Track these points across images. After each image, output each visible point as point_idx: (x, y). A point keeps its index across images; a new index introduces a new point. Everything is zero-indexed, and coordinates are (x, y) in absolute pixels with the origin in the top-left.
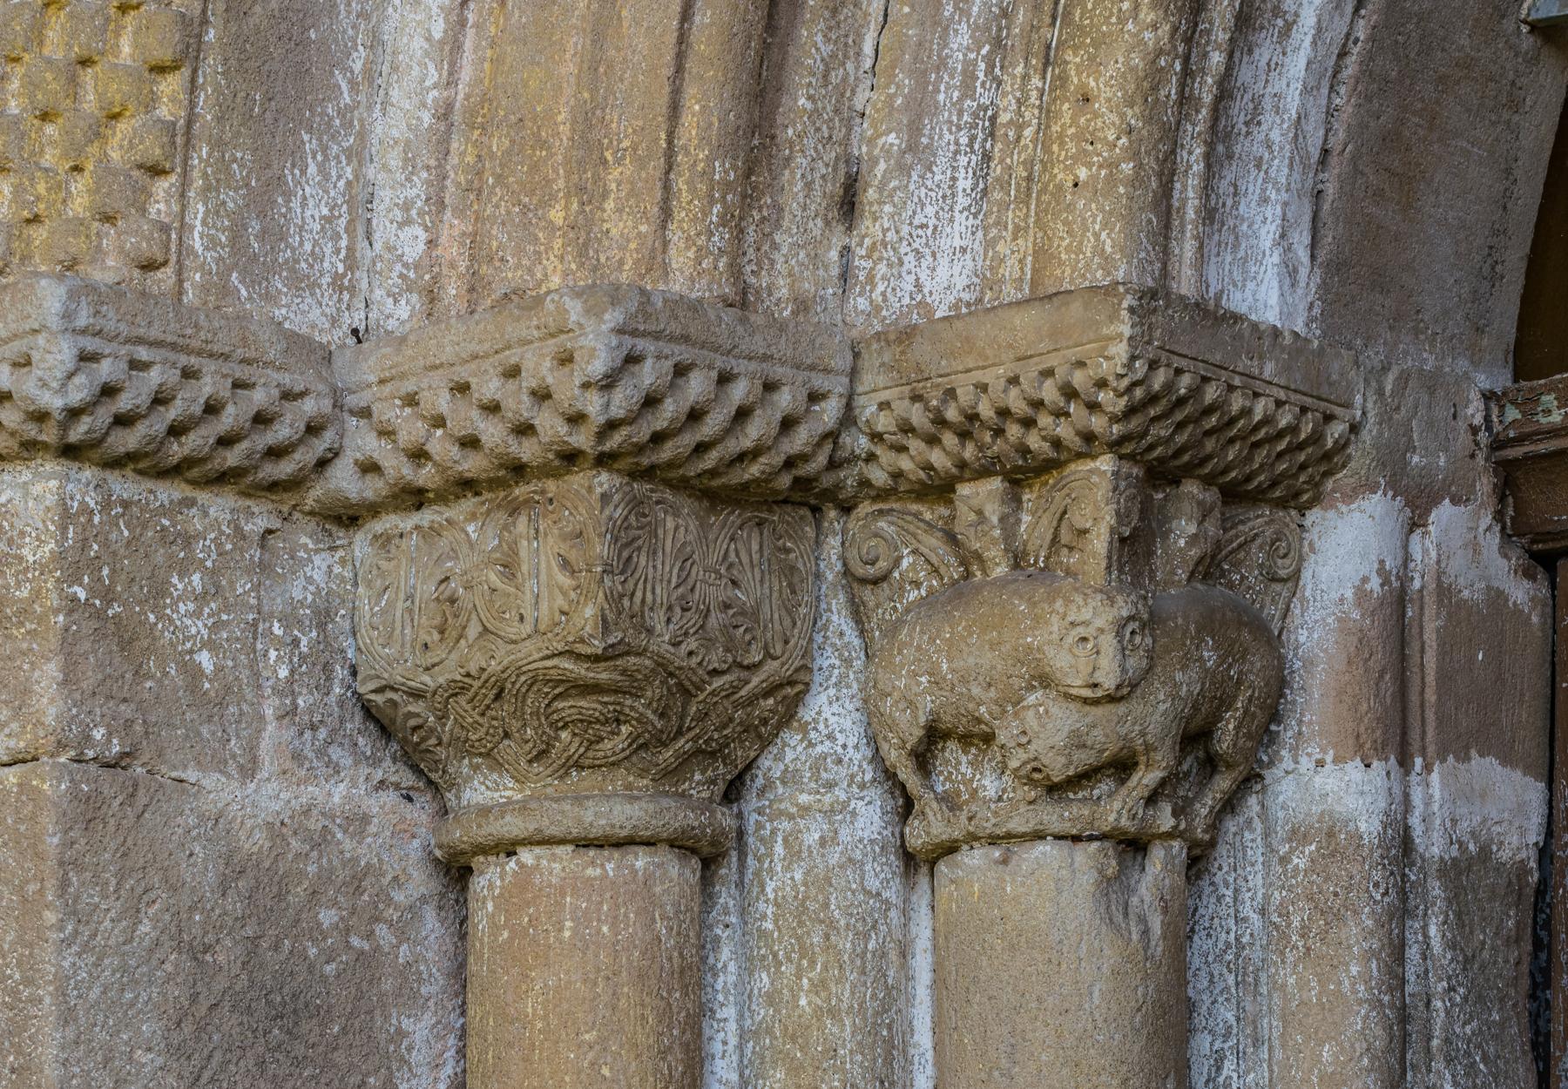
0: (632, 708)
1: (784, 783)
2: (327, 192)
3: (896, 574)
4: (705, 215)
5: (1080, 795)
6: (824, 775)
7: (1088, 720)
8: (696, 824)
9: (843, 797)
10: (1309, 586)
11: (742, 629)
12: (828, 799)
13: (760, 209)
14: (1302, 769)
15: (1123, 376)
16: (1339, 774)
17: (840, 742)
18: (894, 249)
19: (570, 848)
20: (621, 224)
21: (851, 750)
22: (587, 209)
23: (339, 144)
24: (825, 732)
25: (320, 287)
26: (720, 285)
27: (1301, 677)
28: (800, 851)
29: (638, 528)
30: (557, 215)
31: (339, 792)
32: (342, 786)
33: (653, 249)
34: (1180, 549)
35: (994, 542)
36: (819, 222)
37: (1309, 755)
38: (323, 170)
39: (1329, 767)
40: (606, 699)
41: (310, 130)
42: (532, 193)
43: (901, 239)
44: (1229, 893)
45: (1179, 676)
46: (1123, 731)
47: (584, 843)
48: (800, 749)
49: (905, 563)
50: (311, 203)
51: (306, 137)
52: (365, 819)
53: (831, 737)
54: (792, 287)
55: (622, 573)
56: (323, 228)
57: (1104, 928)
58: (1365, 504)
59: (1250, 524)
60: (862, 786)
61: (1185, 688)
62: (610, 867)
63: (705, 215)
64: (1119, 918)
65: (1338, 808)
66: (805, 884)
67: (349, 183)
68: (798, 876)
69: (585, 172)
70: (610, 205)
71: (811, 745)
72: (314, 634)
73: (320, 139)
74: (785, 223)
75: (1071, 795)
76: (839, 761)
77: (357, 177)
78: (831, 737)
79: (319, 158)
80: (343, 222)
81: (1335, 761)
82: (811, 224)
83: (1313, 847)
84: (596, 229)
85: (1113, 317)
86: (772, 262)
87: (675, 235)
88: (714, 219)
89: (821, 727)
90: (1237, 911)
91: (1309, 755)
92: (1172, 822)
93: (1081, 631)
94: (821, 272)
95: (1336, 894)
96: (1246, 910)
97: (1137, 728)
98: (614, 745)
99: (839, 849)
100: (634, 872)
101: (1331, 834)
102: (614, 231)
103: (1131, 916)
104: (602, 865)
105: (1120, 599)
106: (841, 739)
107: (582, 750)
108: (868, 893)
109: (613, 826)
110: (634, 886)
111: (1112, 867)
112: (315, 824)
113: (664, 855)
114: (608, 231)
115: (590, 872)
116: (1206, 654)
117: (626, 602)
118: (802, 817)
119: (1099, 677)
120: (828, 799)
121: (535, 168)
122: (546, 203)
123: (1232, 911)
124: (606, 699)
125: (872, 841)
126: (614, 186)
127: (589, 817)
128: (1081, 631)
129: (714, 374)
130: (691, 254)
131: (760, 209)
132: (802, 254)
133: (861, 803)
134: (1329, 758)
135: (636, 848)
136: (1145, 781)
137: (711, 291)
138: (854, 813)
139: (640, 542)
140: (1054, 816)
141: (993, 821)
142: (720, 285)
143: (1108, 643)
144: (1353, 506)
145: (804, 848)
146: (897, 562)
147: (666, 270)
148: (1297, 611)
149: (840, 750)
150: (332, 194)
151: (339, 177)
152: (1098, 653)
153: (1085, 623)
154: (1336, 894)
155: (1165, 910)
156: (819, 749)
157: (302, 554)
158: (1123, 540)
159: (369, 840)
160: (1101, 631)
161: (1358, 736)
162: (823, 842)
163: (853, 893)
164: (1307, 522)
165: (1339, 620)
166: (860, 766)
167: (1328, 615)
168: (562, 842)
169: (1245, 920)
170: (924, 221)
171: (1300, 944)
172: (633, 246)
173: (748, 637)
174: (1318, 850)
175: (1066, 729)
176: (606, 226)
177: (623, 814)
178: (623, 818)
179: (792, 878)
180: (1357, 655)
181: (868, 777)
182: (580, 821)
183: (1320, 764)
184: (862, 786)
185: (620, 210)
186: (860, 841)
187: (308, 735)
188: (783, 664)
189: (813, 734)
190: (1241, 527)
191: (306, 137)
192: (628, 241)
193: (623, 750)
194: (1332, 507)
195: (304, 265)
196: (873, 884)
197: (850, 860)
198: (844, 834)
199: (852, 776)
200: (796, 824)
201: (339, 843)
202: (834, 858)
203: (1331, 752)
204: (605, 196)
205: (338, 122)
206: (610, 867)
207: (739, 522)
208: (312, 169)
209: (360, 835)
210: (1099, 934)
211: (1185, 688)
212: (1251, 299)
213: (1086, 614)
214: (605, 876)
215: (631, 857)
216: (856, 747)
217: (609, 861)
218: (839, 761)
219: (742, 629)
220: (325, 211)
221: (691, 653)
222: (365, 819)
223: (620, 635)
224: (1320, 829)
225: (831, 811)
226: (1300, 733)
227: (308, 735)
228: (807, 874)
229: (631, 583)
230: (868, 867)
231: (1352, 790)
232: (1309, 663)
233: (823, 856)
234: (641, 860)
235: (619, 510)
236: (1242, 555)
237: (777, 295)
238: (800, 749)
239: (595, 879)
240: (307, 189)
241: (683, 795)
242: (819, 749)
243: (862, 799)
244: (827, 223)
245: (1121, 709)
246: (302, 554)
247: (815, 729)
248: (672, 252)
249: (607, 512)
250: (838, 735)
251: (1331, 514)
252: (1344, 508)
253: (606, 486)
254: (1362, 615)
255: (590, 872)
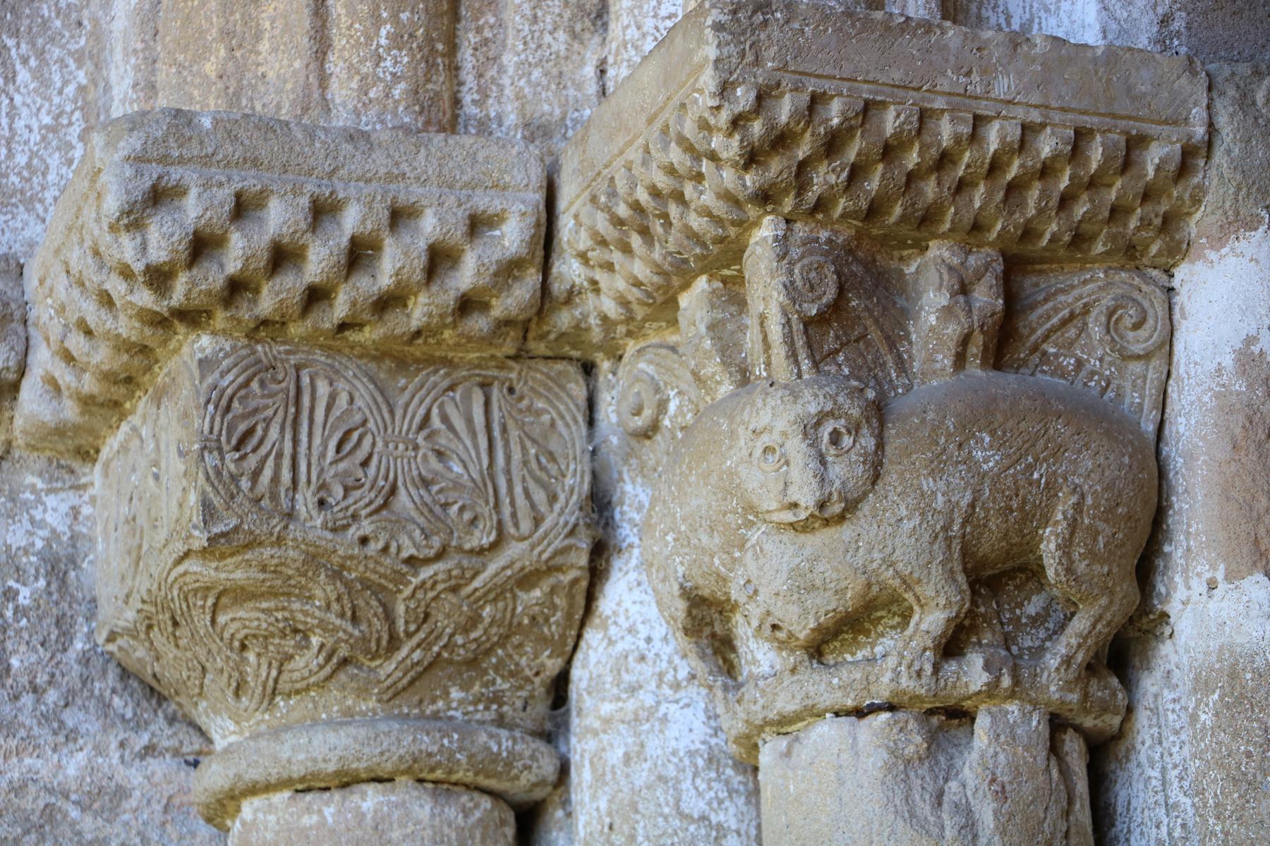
0: (306, 613)
1: (589, 693)
2: (49, 99)
3: (667, 422)
4: (369, 39)
5: (859, 655)
6: (626, 677)
7: (807, 552)
8: (435, 748)
9: (649, 701)
10: (1182, 361)
11: (455, 508)
12: (631, 705)
13: (479, 30)
14: (1195, 598)
15: (718, 108)
16: (1236, 595)
17: (643, 635)
18: (636, 48)
19: (287, 794)
20: (277, 65)
21: (657, 644)
22: (238, 54)
23: (63, 47)
24: (626, 625)
25: (41, 201)
26: (395, 114)
27: (1183, 476)
28: (604, 774)
29: (263, 396)
30: (210, 68)
31: (74, 765)
32: (80, 756)
33: (307, 86)
34: (932, 329)
35: (707, 355)
36: (562, 35)
37: (1199, 575)
38: (37, 74)
39: (1222, 586)
40: (265, 605)
41: (16, 34)
42: (185, 49)
43: (644, 35)
44: (1155, 773)
45: (927, 484)
46: (860, 561)
47: (308, 785)
48: (601, 649)
49: (672, 407)
50: (25, 112)
51: (10, 42)
52: (121, 793)
53: (631, 630)
54: (522, 111)
55: (237, 449)
56: (44, 138)
57: (900, 822)
58: (1242, 245)
59: (1076, 293)
60: (676, 686)
61: (940, 499)
62: (329, 812)
63: (369, 39)
64: (924, 808)
65: (1240, 640)
66: (610, 814)
67: (82, 89)
68: (603, 805)
69: (232, 14)
70: (264, 46)
71: (611, 642)
72: (42, 583)
73: (33, 44)
74: (510, 41)
75: (849, 657)
76: (642, 658)
77: (94, 82)
78: (631, 630)
79: (33, 62)
80: (76, 130)
81: (1229, 578)
82: (547, 38)
83: (1216, 696)
84: (249, 75)
85: (701, 41)
86: (501, 88)
87: (335, 65)
88: (383, 42)
89: (621, 620)
90: (1166, 796)
91: (1199, 575)
92: (985, 677)
93: (766, 439)
94: (571, 92)
95: (1249, 755)
96: (1176, 795)
97: (876, 555)
98: (305, 663)
99: (646, 766)
100: (361, 816)
101: (1233, 675)
102: (271, 75)
103: (945, 806)
104: (320, 811)
105: (807, 395)
106: (643, 631)
107: (274, 673)
108: (688, 818)
109: (315, 760)
110: (359, 833)
111: (915, 742)
112: (32, 802)
113: (404, 791)
114: (264, 76)
115: (307, 821)
116: (979, 455)
117: (245, 484)
118: (605, 732)
119: (794, 495)
120: (631, 705)
121: (188, 20)
122: (200, 57)
123: (1160, 797)
124: (265, 605)
125: (691, 754)
126: (267, 25)
127: (285, 752)
128: (766, 439)
129: (304, 201)
130: (354, 85)
131: (479, 30)
132: (536, 74)
133: (673, 707)
134: (1220, 575)
135: (364, 787)
136: (924, 626)
137: (383, 122)
138: (665, 719)
139: (270, 412)
140: (826, 686)
141: (761, 702)
142: (395, 114)
143: (796, 447)
144: (1224, 251)
145: (608, 769)
146: (662, 406)
147: (326, 107)
148: (1175, 396)
149: (642, 645)
150: (56, 100)
151: (66, 83)
152: (787, 463)
153: (767, 429)
154: (1249, 755)
155: (1001, 794)
156: (620, 646)
157: (28, 496)
158: (808, 323)
159: (126, 817)
160: (784, 434)
161: (1256, 542)
162: (627, 759)
163: (666, 818)
164: (1176, 283)
165: (1217, 396)
166: (670, 662)
167: (1204, 392)
168: (268, 788)
169: (1176, 806)
170: (673, 10)
171: (1218, 828)
172: (289, 86)
173: (467, 516)
174: (1221, 698)
175: (785, 568)
176: (261, 70)
177: (325, 747)
178: (325, 750)
179: (598, 809)
180: (1246, 438)
181: (683, 673)
182: (276, 759)
183: (1212, 586)
184: (676, 686)
185: (275, 50)
186: (674, 753)
187: (27, 700)
188: (533, 548)
189: (613, 630)
190: (1062, 298)
191: (10, 42)
192: (285, 82)
193: (321, 667)
194: (1199, 257)
195: (14, 179)
196: (694, 805)
197: (660, 778)
198: (653, 747)
199: (661, 676)
200: (600, 741)
201: (73, 823)
202: (642, 775)
203: (1222, 567)
204: (258, 38)
205: (58, 23)
206: (329, 812)
207: (446, 383)
208: (23, 75)
209: (112, 812)
210: (893, 832)
211: (940, 499)
212: (1066, 22)
213: (765, 418)
214: (323, 822)
215: (356, 798)
216: (665, 639)
217: (327, 804)
218: (642, 658)
219: (455, 508)
220: (47, 120)
221: (364, 541)
222: (121, 793)
223: (234, 522)
224: (1221, 670)
225: (636, 720)
226: (1189, 549)
227: (27, 700)
228: (610, 801)
229: (252, 461)
230: (686, 785)
231: (1254, 613)
232: (1190, 457)
233: (628, 776)
234: (370, 799)
235: (230, 377)
236: (1072, 332)
237: (507, 123)
238: (601, 649)
239: (311, 828)
240: (18, 99)
241: (436, 716)
242: (620, 646)
243: (677, 702)
244: (574, 35)
245: (846, 532)
246: (28, 496)
247: (615, 623)
248: (334, 84)
249: (210, 380)
250: (640, 627)
251: (1199, 266)
252: (1212, 255)
253: (208, 351)
254: (1249, 386)
255: (307, 821)
